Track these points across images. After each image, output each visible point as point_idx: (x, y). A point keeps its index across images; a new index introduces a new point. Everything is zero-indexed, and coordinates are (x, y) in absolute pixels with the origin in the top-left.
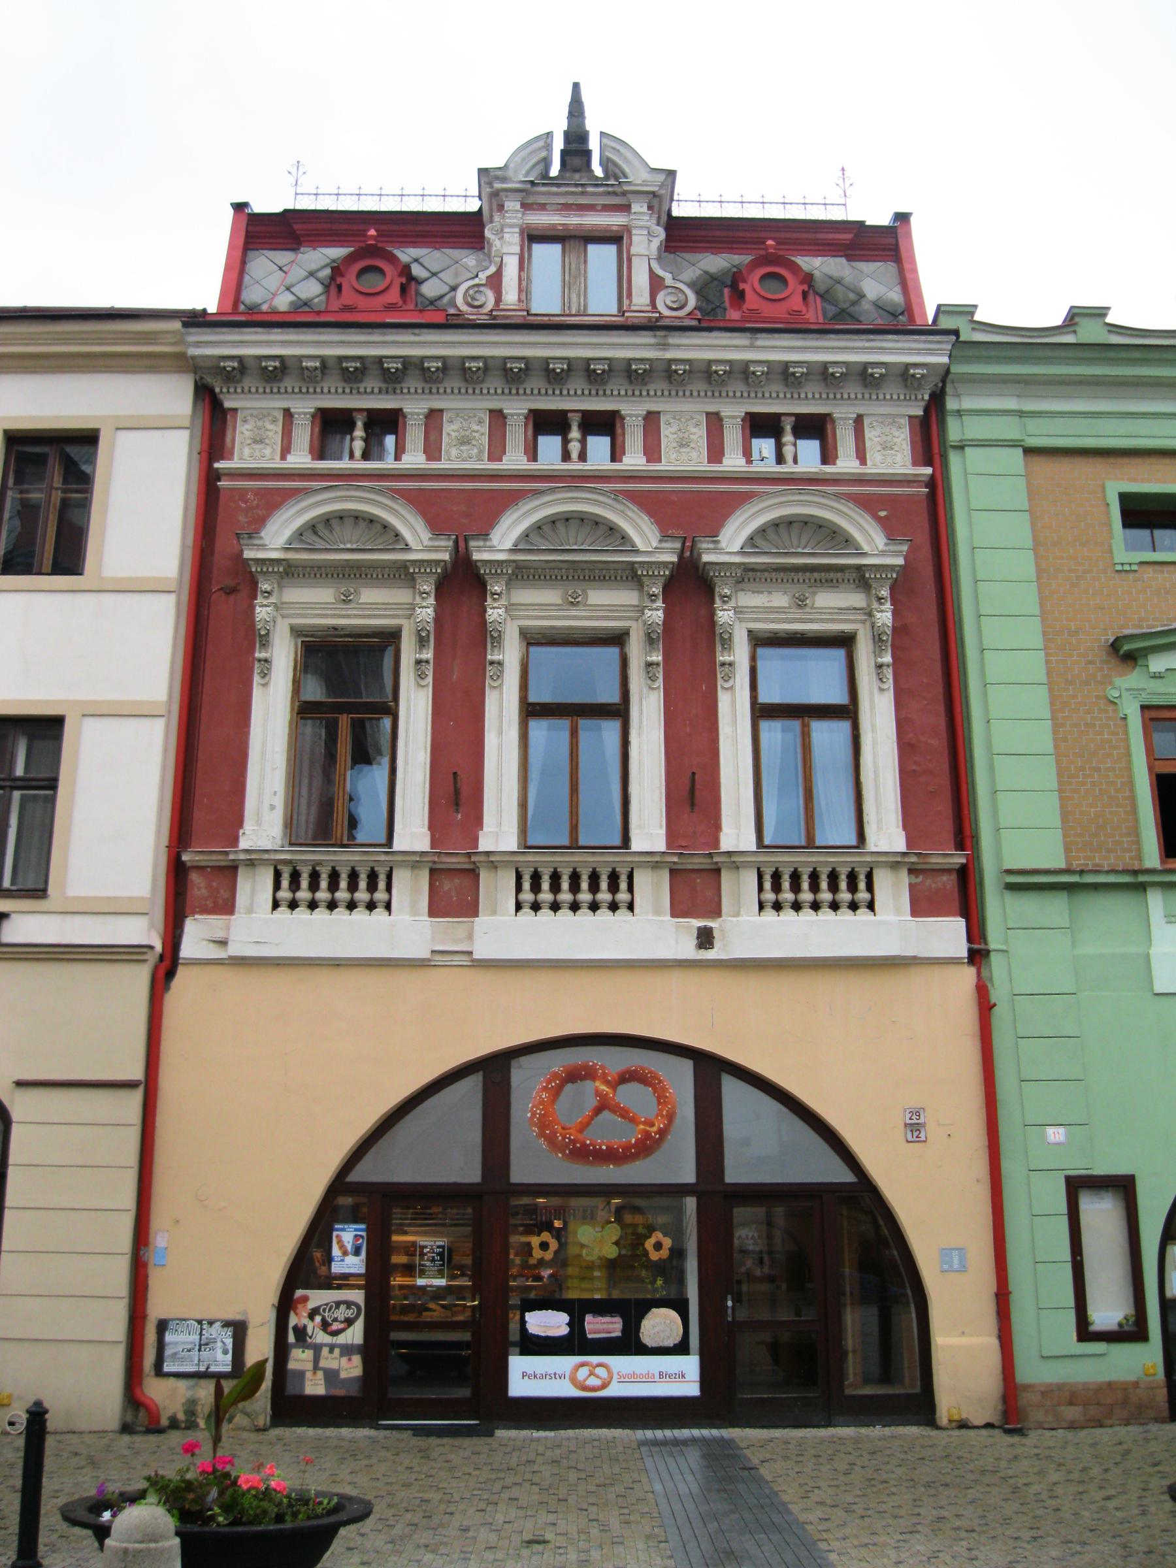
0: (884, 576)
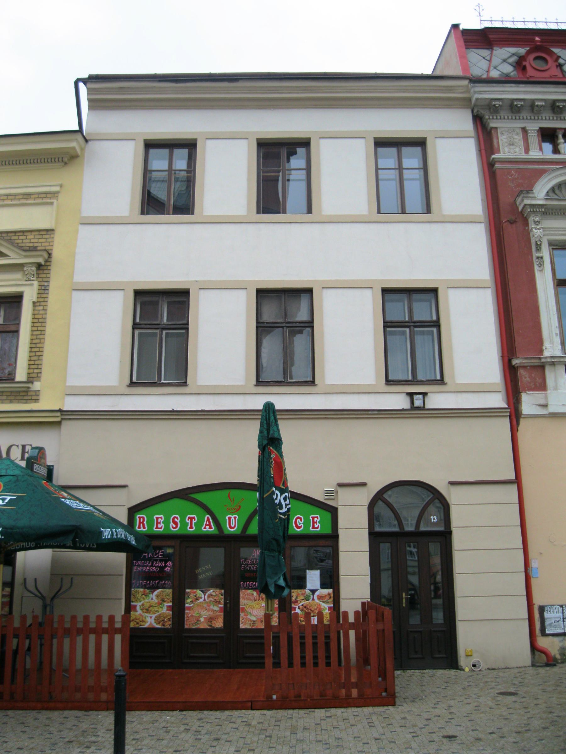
0: (532, 210)
